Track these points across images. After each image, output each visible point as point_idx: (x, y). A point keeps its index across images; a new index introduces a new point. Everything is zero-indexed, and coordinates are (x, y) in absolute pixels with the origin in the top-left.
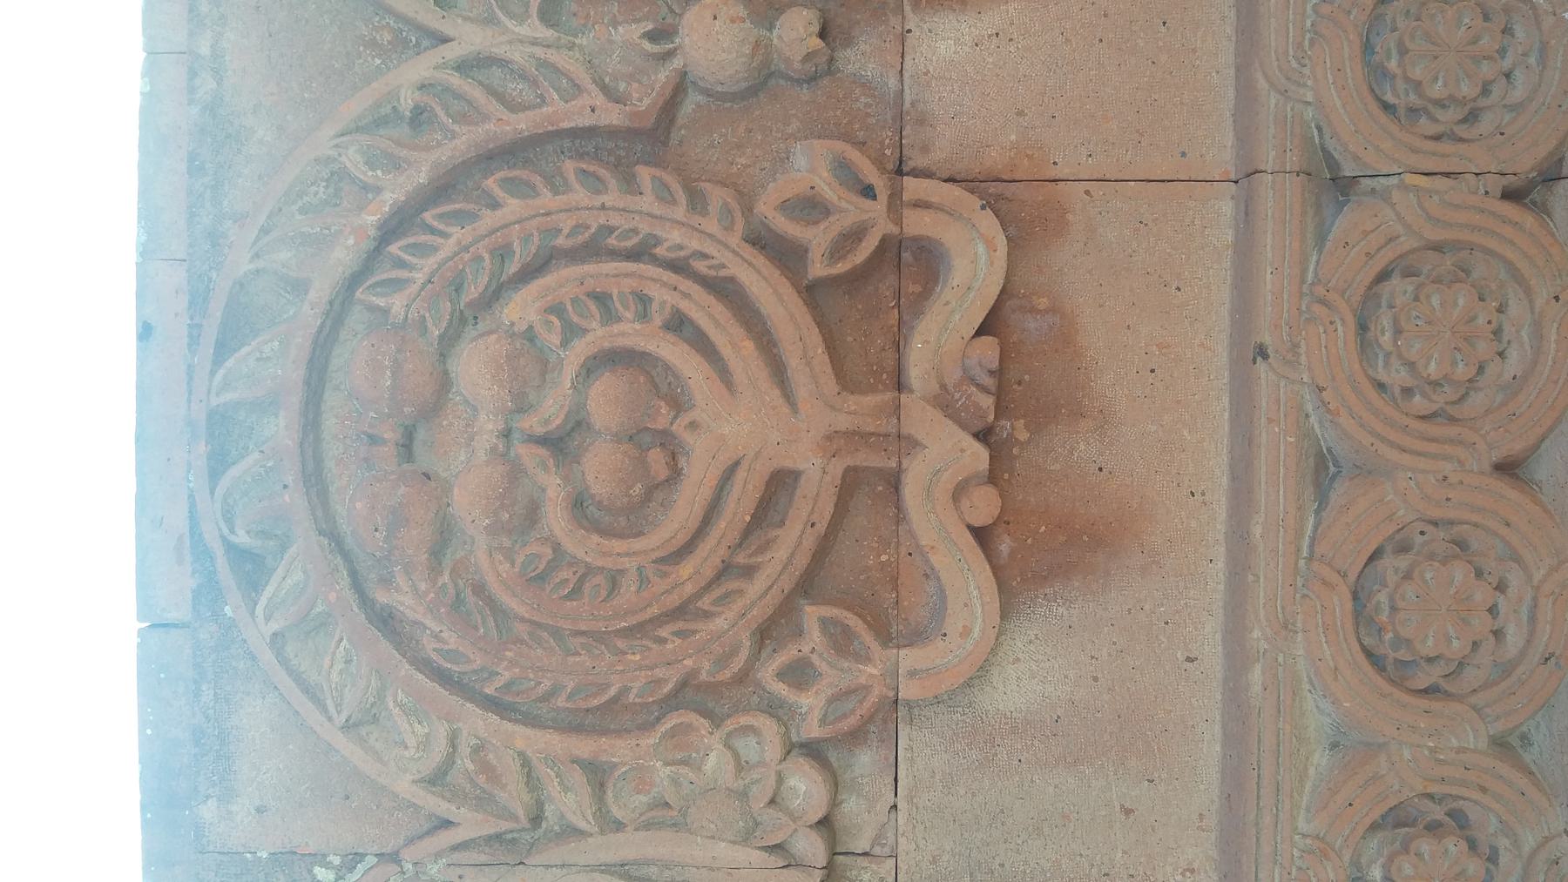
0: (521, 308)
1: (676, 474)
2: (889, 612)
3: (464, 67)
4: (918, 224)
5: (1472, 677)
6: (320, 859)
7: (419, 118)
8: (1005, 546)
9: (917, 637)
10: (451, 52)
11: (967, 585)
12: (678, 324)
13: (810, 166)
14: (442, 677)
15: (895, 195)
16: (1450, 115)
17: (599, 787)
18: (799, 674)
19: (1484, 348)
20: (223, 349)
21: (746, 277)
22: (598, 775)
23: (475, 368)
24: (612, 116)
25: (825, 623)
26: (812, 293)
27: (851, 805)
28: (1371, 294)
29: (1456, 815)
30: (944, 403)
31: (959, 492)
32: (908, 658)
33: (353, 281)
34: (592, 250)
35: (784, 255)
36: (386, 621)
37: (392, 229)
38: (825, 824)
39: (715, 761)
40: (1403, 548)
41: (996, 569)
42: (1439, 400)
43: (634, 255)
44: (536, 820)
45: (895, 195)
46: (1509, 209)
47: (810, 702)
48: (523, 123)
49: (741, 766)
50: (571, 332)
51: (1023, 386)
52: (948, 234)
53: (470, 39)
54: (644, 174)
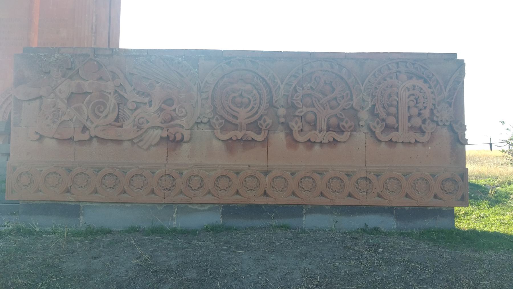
0: (255, 92)
1: (238, 107)
2: (223, 129)
3: (279, 86)
4: (263, 132)
5: (216, 188)
6: (198, 69)
7: (274, 82)
8: (230, 142)
9: (221, 132)
10: (281, 85)
11: (226, 137)
12: (253, 108)
13: (269, 121)
14: (217, 83)
15: (266, 130)
16: (188, 184)
17: (205, 99)
18: (217, 119)
19: (250, 188)
20: (251, 61)
21: (258, 114)
22: (207, 99)
23: (249, 87)
24: (274, 101)
25: (222, 122)
26: (256, 122)
27: (203, 125)
28: (282, 178)
29: (202, 187)
30: (245, 135)
31: (236, 136)
32: (219, 131)
33: (258, 75)
34: (261, 99)
35: (260, 119)
36: (223, 77)
37: (263, 78)
38: (202, 122)
39: (208, 111)
40: (230, 181)
41: (228, 140)
42: (301, 185)
43: (260, 103)
44: (202, 92)
45: (266, 130)
46: (263, 191)
47: (214, 121)
48: (273, 92)
49: (208, 113)
50: (252, 97)
51: (247, 143)
52: (262, 135)
53: (282, 87)
54: (268, 104)
